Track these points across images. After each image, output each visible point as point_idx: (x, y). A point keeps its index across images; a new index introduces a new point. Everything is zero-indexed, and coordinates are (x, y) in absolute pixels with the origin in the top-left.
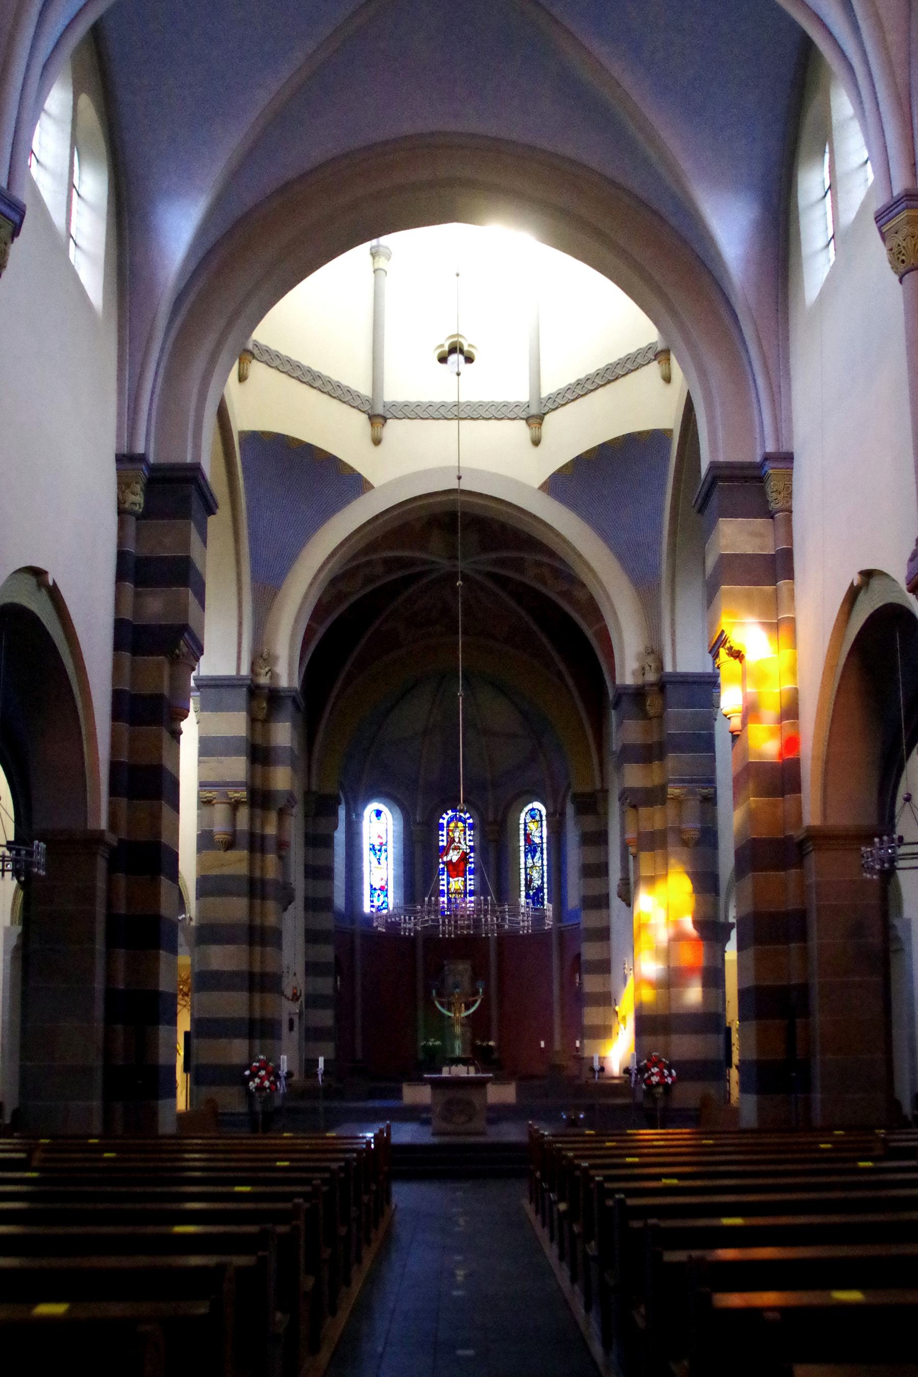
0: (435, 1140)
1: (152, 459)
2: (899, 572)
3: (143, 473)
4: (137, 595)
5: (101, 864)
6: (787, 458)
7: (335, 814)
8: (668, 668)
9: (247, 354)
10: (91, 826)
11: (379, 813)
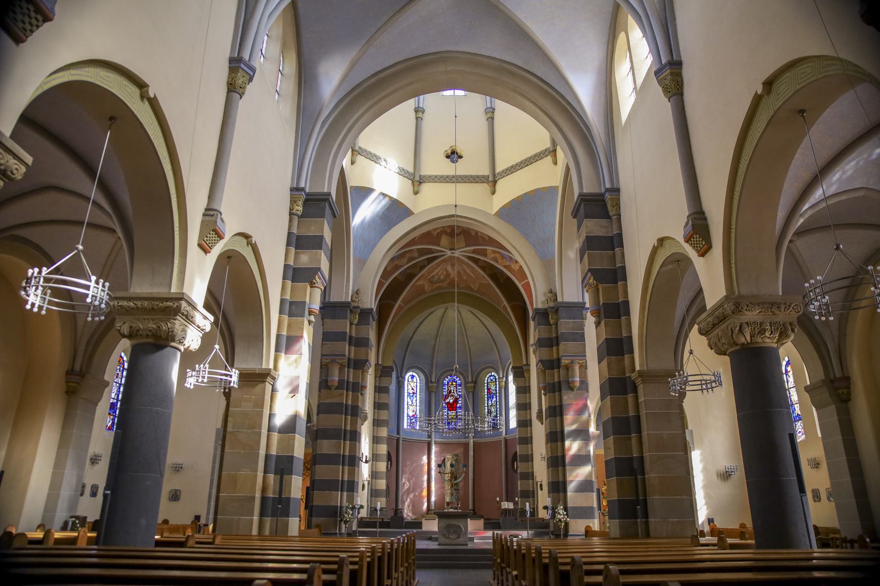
0: (438, 547)
1: (307, 191)
2: (679, 235)
3: (303, 197)
4: (296, 253)
6: (616, 191)
8: (559, 300)
9: (356, 152)
11: (413, 377)
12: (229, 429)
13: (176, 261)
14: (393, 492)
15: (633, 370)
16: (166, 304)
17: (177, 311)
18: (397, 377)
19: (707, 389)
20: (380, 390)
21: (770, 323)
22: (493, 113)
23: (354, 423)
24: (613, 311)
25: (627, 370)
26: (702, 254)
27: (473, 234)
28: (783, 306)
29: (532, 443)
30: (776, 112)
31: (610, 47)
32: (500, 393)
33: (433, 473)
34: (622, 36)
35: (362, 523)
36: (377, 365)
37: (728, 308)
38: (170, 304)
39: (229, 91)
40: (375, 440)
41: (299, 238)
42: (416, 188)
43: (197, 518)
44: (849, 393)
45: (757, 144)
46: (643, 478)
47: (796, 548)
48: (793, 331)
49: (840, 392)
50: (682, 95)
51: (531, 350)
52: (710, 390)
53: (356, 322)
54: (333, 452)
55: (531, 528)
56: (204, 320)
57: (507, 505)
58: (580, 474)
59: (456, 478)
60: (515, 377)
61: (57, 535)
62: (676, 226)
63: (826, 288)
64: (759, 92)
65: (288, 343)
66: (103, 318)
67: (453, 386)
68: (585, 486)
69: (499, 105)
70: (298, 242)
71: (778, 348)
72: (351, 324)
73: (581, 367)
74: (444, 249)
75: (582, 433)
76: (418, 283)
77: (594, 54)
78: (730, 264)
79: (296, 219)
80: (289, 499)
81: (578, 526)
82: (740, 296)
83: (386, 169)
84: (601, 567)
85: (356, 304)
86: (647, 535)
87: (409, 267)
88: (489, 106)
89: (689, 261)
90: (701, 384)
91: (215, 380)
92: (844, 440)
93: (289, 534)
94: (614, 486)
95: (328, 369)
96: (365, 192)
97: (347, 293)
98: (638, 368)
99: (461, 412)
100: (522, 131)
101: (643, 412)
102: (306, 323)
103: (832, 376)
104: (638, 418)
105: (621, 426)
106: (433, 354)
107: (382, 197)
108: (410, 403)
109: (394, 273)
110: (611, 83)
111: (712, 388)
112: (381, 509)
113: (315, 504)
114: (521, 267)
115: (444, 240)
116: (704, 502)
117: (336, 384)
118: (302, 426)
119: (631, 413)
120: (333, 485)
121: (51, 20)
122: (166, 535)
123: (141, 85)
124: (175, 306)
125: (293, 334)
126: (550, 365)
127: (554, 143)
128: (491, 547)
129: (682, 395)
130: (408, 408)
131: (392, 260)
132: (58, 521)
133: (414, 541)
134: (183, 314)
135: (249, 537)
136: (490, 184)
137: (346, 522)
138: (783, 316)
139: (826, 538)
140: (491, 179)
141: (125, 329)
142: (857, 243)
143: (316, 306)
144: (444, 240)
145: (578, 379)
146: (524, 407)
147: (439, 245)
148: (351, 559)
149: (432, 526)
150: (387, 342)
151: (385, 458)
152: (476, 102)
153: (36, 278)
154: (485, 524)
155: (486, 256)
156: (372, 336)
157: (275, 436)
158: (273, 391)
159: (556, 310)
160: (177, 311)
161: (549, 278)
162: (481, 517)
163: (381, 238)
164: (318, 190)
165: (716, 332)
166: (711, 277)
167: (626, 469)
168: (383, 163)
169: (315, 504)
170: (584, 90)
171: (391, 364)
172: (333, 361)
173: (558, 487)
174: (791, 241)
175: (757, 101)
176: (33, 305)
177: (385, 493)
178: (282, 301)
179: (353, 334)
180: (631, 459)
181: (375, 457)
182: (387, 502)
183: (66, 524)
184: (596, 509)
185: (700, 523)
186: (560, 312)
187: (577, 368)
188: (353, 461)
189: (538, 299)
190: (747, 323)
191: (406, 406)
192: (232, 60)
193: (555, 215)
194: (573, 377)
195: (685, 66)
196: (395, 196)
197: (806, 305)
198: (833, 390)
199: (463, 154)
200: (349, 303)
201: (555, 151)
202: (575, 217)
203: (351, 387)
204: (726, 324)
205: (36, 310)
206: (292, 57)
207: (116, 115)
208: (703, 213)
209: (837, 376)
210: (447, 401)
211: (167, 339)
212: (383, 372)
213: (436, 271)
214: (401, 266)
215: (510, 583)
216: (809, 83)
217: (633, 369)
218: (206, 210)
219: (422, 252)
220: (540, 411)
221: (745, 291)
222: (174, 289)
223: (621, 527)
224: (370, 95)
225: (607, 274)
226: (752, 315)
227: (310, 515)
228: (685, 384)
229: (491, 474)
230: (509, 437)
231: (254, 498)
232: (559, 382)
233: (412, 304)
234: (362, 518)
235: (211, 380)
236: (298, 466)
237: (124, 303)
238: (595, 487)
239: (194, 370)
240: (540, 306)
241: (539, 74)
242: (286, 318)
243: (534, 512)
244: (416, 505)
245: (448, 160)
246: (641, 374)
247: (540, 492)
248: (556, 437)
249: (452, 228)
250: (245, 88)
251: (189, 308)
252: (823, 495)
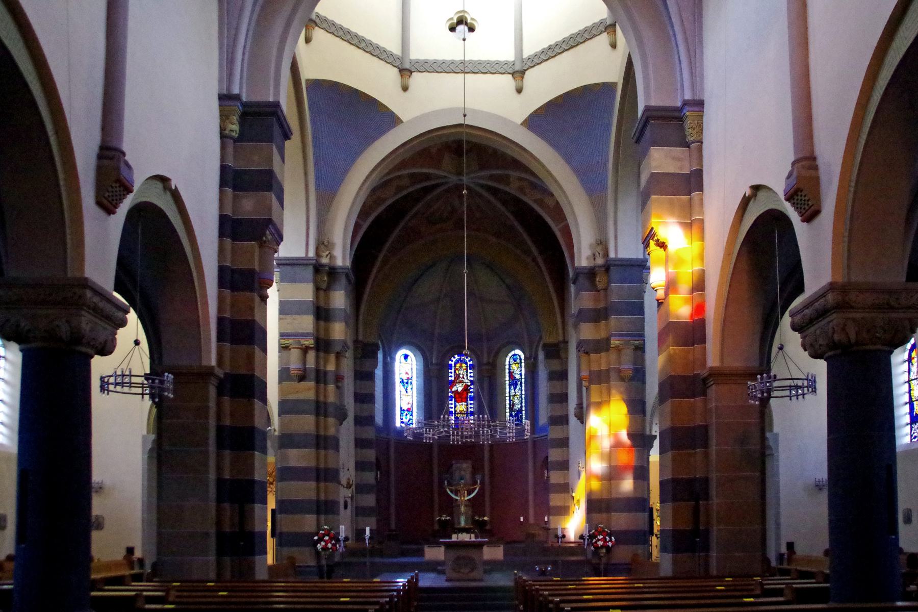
0: (447, 584)
1: (244, 99)
2: (779, 186)
3: (238, 109)
4: (235, 198)
5: (212, 391)
7: (376, 357)
8: (612, 255)
10: (204, 363)
11: (406, 357)
43: (130, 551)
53: (324, 286)
70: (233, 179)
79: (230, 149)
111: (803, 394)
115: (447, 160)
129: (765, 402)
134: (89, 307)
155: (508, 184)
165: (812, 329)
189: (583, 255)
201: (613, 26)
204: (826, 320)
208: (814, 159)
210: (454, 389)
214: (384, 200)
223: (675, 562)
249: (459, 143)
251: (96, 299)
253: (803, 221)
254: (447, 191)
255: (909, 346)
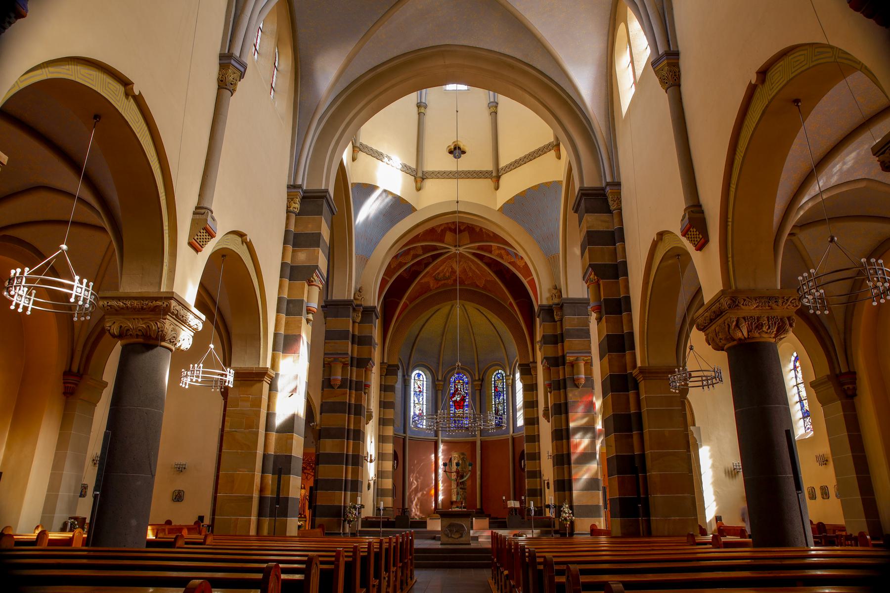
0: (440, 547)
2: (677, 229)
4: (293, 251)
7: (397, 375)
8: (564, 296)
11: (419, 375)
12: (226, 429)
13: (166, 260)
14: (400, 490)
15: (635, 366)
16: (155, 303)
17: (167, 311)
18: (404, 376)
19: (708, 385)
20: (385, 388)
21: (768, 318)
22: (496, 107)
23: (358, 422)
24: (615, 307)
25: (628, 368)
26: (700, 248)
27: (478, 230)
28: (780, 301)
29: (539, 441)
30: (769, 103)
31: (610, 38)
32: (507, 391)
33: (441, 471)
34: (622, 26)
35: (367, 522)
36: (382, 363)
37: (725, 302)
38: (159, 303)
39: (220, 88)
40: (381, 439)
41: (296, 236)
42: (419, 185)
43: (201, 518)
44: (855, 389)
45: (752, 135)
46: (646, 475)
47: (789, 546)
48: (791, 325)
49: (846, 387)
50: (679, 86)
51: (538, 347)
52: (711, 387)
53: (358, 320)
54: (336, 451)
55: (536, 527)
56: (196, 320)
57: (513, 504)
58: (584, 474)
59: (462, 477)
60: (521, 374)
61: (53, 536)
62: (673, 220)
63: (823, 280)
64: (753, 82)
65: (287, 343)
66: (88, 318)
67: (461, 384)
68: (592, 484)
69: (502, 99)
70: (295, 240)
71: (776, 343)
72: (354, 322)
73: (586, 363)
74: (451, 247)
75: (588, 429)
76: (423, 281)
77: (594, 46)
78: (727, 257)
79: (293, 218)
80: (287, 499)
81: (583, 525)
82: (737, 291)
83: (384, 168)
84: (564, 567)
85: (359, 303)
86: (649, 534)
87: (413, 265)
88: (492, 100)
89: (687, 254)
90: (702, 381)
91: (211, 380)
92: (849, 436)
93: (288, 534)
94: (616, 484)
95: (331, 367)
96: (369, 189)
97: (350, 291)
98: (639, 364)
99: (467, 410)
100: (524, 126)
101: (644, 409)
102: (304, 321)
103: (838, 372)
104: (639, 415)
105: (623, 424)
106: (440, 352)
107: (384, 195)
108: (417, 401)
109: (398, 270)
110: (611, 75)
111: (713, 384)
112: (385, 509)
113: (318, 503)
114: (526, 263)
116: (713, 498)
117: (339, 383)
118: (300, 426)
119: (633, 410)
120: (336, 485)
121: (23, 16)
122: (161, 535)
123: (126, 83)
124: (165, 305)
125: (290, 332)
126: (555, 362)
127: (557, 139)
128: (490, 546)
129: (684, 391)
130: (415, 406)
131: (396, 257)
132: (58, 522)
133: (412, 541)
135: (247, 537)
136: (494, 179)
137: (349, 522)
138: (780, 311)
139: (824, 534)
140: (494, 174)
141: (115, 330)
142: (859, 237)
143: (314, 304)
144: (449, 236)
145: (583, 376)
146: (530, 405)
147: (443, 242)
148: (321, 559)
149: (435, 525)
150: (392, 341)
151: (391, 457)
152: (480, 97)
153: (18, 278)
154: (490, 523)
155: (491, 252)
156: (376, 334)
157: (273, 436)
158: (270, 390)
159: (561, 306)
160: (167, 311)
161: (554, 275)
162: (488, 516)
163: (383, 235)
164: (315, 187)
166: (708, 272)
167: (627, 467)
168: (386, 160)
169: (318, 503)
170: (584, 83)
171: (396, 362)
172: (335, 360)
173: (564, 485)
174: (790, 234)
175: (752, 91)
176: (17, 305)
177: (391, 493)
178: (280, 300)
179: (356, 333)
180: (632, 457)
181: (381, 456)
182: (394, 502)
183: (65, 524)
184: (602, 508)
185: (708, 520)
186: (564, 308)
187: (582, 365)
188: (358, 460)
189: (542, 296)
190: (744, 318)
191: (412, 405)
192: (222, 57)
193: (558, 209)
194: (578, 373)
195: (682, 57)
196: (398, 192)
197: (800, 299)
198: (837, 386)
199: (466, 149)
200: (352, 301)
201: (558, 145)
202: (576, 212)
203: (354, 386)
205: (20, 310)
206: (288, 52)
207: (100, 113)
208: (700, 206)
209: (843, 371)
211: (157, 339)
212: (388, 370)
213: (440, 268)
214: (406, 264)
215: (390, 590)
216: (799, 74)
217: (634, 366)
218: (197, 208)
219: (426, 249)
220: (546, 409)
221: (742, 285)
222: (164, 289)
224: (370, 89)
225: (608, 270)
226: (750, 309)
227: (314, 515)
228: (685, 380)
229: (499, 473)
230: (516, 435)
231: (251, 498)
232: (565, 380)
233: (418, 301)
234: (367, 518)
235: (206, 380)
236: (297, 465)
237: (114, 303)
238: (601, 485)
239: (188, 370)
240: (545, 302)
241: (539, 67)
242: (283, 316)
243: (540, 511)
244: (423, 504)
245: (451, 156)
246: (642, 371)
247: (547, 490)
248: (562, 435)
250: (236, 84)
251: (179, 308)
252: (832, 492)
253: (697, 250)
254: (449, 258)
255: (793, 358)
